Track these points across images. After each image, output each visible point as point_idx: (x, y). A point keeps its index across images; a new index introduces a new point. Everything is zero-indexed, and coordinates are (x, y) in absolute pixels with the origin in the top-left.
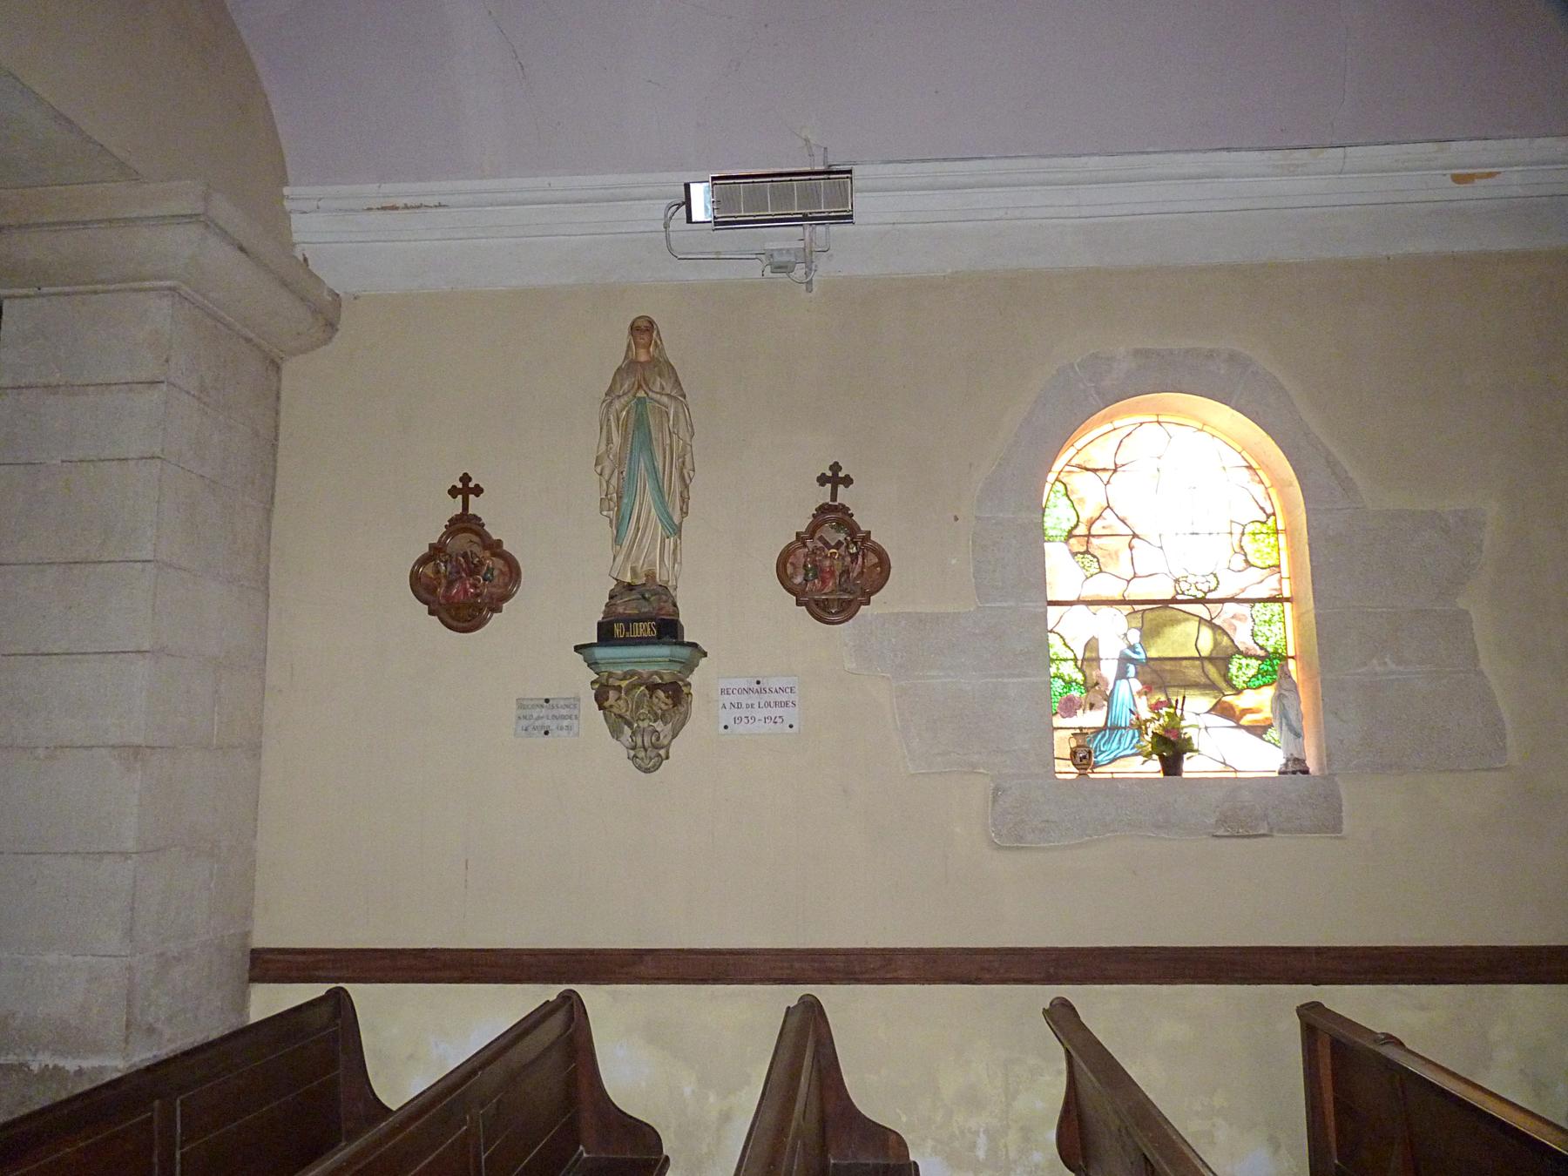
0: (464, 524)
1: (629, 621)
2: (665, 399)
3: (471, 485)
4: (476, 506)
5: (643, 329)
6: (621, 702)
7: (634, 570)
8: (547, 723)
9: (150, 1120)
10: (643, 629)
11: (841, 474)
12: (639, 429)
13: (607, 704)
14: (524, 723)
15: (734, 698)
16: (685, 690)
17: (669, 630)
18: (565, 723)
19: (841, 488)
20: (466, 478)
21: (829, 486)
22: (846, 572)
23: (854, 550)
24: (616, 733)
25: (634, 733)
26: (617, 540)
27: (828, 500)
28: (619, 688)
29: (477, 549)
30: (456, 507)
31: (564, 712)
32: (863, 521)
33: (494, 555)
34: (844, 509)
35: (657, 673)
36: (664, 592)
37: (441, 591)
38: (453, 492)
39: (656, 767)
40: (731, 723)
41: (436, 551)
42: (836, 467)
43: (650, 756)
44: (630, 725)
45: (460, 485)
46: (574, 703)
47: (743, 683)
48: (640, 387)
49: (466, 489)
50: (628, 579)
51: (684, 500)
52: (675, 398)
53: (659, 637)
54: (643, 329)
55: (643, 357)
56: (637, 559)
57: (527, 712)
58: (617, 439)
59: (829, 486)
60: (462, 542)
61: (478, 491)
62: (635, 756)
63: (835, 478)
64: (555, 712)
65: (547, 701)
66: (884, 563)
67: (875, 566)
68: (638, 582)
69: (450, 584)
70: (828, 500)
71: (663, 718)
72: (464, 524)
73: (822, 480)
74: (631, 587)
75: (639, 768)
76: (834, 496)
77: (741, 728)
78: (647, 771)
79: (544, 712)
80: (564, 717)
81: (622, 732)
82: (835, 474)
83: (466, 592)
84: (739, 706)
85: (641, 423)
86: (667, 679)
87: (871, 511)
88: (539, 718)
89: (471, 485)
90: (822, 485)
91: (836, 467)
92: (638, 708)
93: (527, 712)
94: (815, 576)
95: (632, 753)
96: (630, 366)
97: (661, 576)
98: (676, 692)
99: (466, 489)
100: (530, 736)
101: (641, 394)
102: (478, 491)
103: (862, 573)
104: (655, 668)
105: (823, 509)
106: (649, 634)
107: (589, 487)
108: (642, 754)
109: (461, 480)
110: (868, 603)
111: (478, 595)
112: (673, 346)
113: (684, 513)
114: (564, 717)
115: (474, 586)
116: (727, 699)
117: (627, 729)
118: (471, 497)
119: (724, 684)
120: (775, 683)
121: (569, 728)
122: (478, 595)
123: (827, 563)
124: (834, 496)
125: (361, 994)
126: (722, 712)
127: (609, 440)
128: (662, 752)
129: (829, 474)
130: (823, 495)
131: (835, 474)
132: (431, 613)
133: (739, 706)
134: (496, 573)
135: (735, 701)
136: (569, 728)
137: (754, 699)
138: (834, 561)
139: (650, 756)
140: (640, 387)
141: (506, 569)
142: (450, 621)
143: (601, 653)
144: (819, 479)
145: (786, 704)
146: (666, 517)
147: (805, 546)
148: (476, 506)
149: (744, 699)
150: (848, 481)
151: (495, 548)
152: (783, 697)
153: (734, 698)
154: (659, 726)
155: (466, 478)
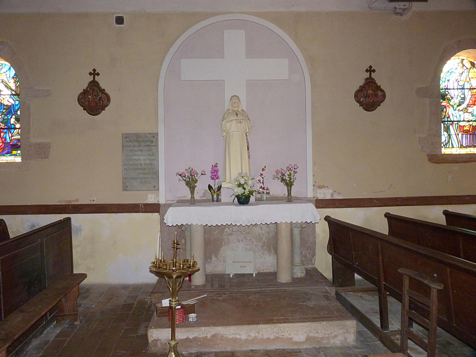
4: (373, 75)
9: (411, 278)
19: (96, 76)
20: (94, 70)
21: (369, 73)
32: (102, 86)
33: (102, 93)
34: (97, 83)
38: (90, 74)
42: (371, 67)
49: (94, 73)
59: (369, 73)
61: (98, 74)
73: (90, 74)
76: (94, 78)
91: (371, 67)
99: (94, 73)
102: (98, 74)
105: (367, 79)
118: (372, 73)
124: (94, 78)
125: (77, 220)
130: (367, 75)
142: (90, 112)
144: (89, 74)
148: (373, 75)
155: (94, 70)
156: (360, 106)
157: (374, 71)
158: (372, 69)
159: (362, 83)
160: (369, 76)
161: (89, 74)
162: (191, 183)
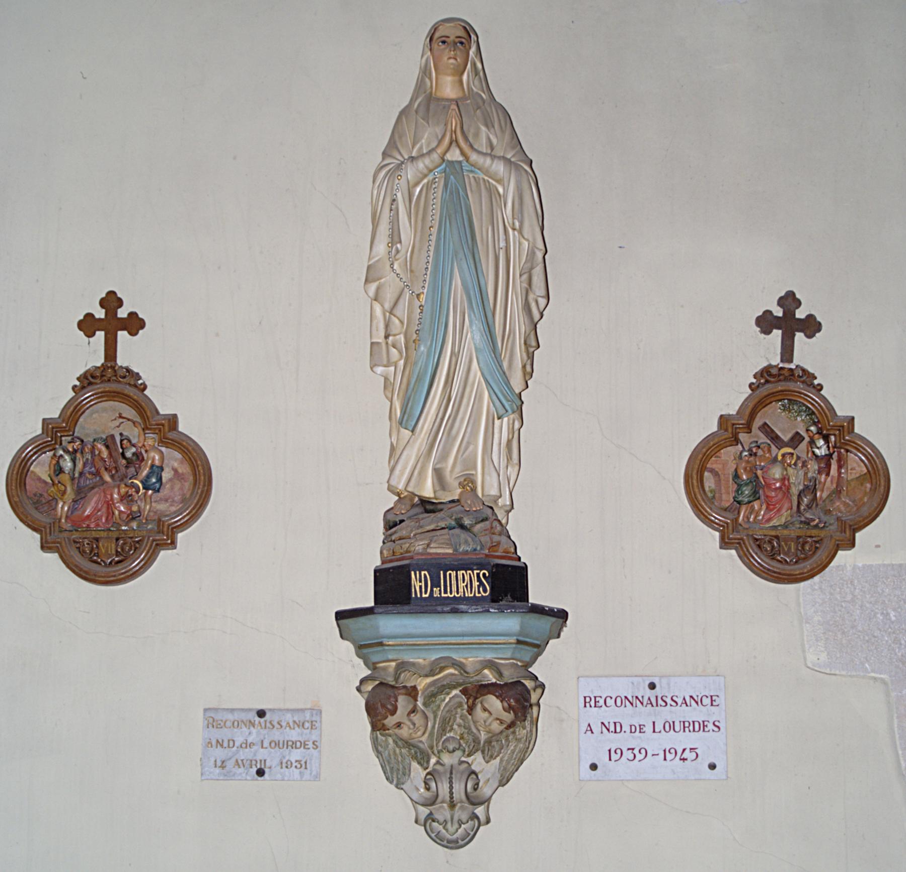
0: (110, 381)
1: (437, 568)
2: (499, 168)
3: (122, 313)
4: (130, 351)
5: (456, 41)
6: (417, 718)
7: (439, 474)
8: (262, 754)
10: (466, 584)
11: (800, 314)
12: (457, 219)
13: (390, 721)
14: (219, 753)
15: (609, 714)
16: (534, 698)
17: (508, 583)
18: (295, 755)
20: (111, 301)
21: (777, 334)
22: (811, 489)
23: (822, 451)
24: (395, 774)
25: (432, 775)
26: (407, 419)
27: (776, 360)
28: (412, 692)
29: (134, 433)
30: (92, 352)
31: (294, 735)
33: (164, 441)
34: (807, 377)
35: (491, 665)
36: (488, 517)
37: (62, 508)
38: (88, 325)
39: (469, 838)
40: (602, 759)
41: (56, 432)
42: (789, 301)
43: (455, 815)
44: (423, 759)
45: (100, 314)
46: (309, 719)
47: (623, 688)
48: (454, 142)
49: (112, 320)
50: (428, 491)
51: (532, 345)
52: (518, 167)
53: (495, 598)
54: (456, 41)
55: (449, 90)
56: (444, 457)
57: (224, 734)
58: (407, 233)
59: (777, 334)
60: (104, 419)
61: (134, 324)
62: (430, 817)
63: (788, 320)
64: (277, 735)
65: (261, 714)
66: (878, 478)
67: (861, 479)
68: (446, 497)
69: (81, 494)
70: (776, 360)
71: (488, 749)
72: (110, 381)
73: (88, 325)
74: (427, 506)
75: (438, 839)
76: (787, 352)
77: (622, 768)
78: (454, 845)
79: (254, 735)
80: (294, 745)
81: (406, 772)
82: (789, 314)
83: (110, 505)
84: (617, 727)
85: (456, 209)
86: (509, 676)
87: (846, 373)
88: (247, 745)
89: (122, 313)
90: (766, 331)
91: (789, 301)
92: (443, 730)
93: (224, 734)
94: (755, 495)
95: (424, 811)
96: (426, 104)
97: (488, 486)
98: (521, 698)
99: (112, 320)
100: (229, 776)
101: (454, 155)
102: (134, 324)
103: (838, 492)
104: (489, 656)
105: (766, 374)
106: (476, 591)
107: (353, 318)
108: (443, 813)
109: (103, 303)
110: (852, 544)
111: (132, 517)
112: (507, 67)
113: (528, 374)
114: (294, 745)
115: (126, 498)
116: (595, 716)
117: (418, 772)
118: (122, 335)
119: (589, 688)
120: (682, 688)
121: (302, 765)
122: (132, 517)
123: (777, 472)
124: (787, 352)
126: (588, 740)
127: (395, 238)
128: (480, 811)
129: (778, 312)
131: (789, 314)
132: (725, 543)
133: (617, 727)
134: (166, 475)
135: (609, 720)
136: (302, 765)
137: (643, 715)
138: (787, 472)
139: (455, 815)
140: (454, 142)
141: (185, 469)
143: (391, 624)
144: (81, 325)
145: (703, 726)
146: (498, 380)
147: (737, 441)
148: (130, 351)
149: (627, 716)
150: (811, 326)
151: (167, 429)
152: (695, 714)
153: (609, 714)
154: (477, 762)
155: (111, 301)
156: (173, 544)
157: (811, 326)
158: (800, 314)
159: (733, 398)
160: (99, 361)
161: (81, 325)
162: (305, 745)
